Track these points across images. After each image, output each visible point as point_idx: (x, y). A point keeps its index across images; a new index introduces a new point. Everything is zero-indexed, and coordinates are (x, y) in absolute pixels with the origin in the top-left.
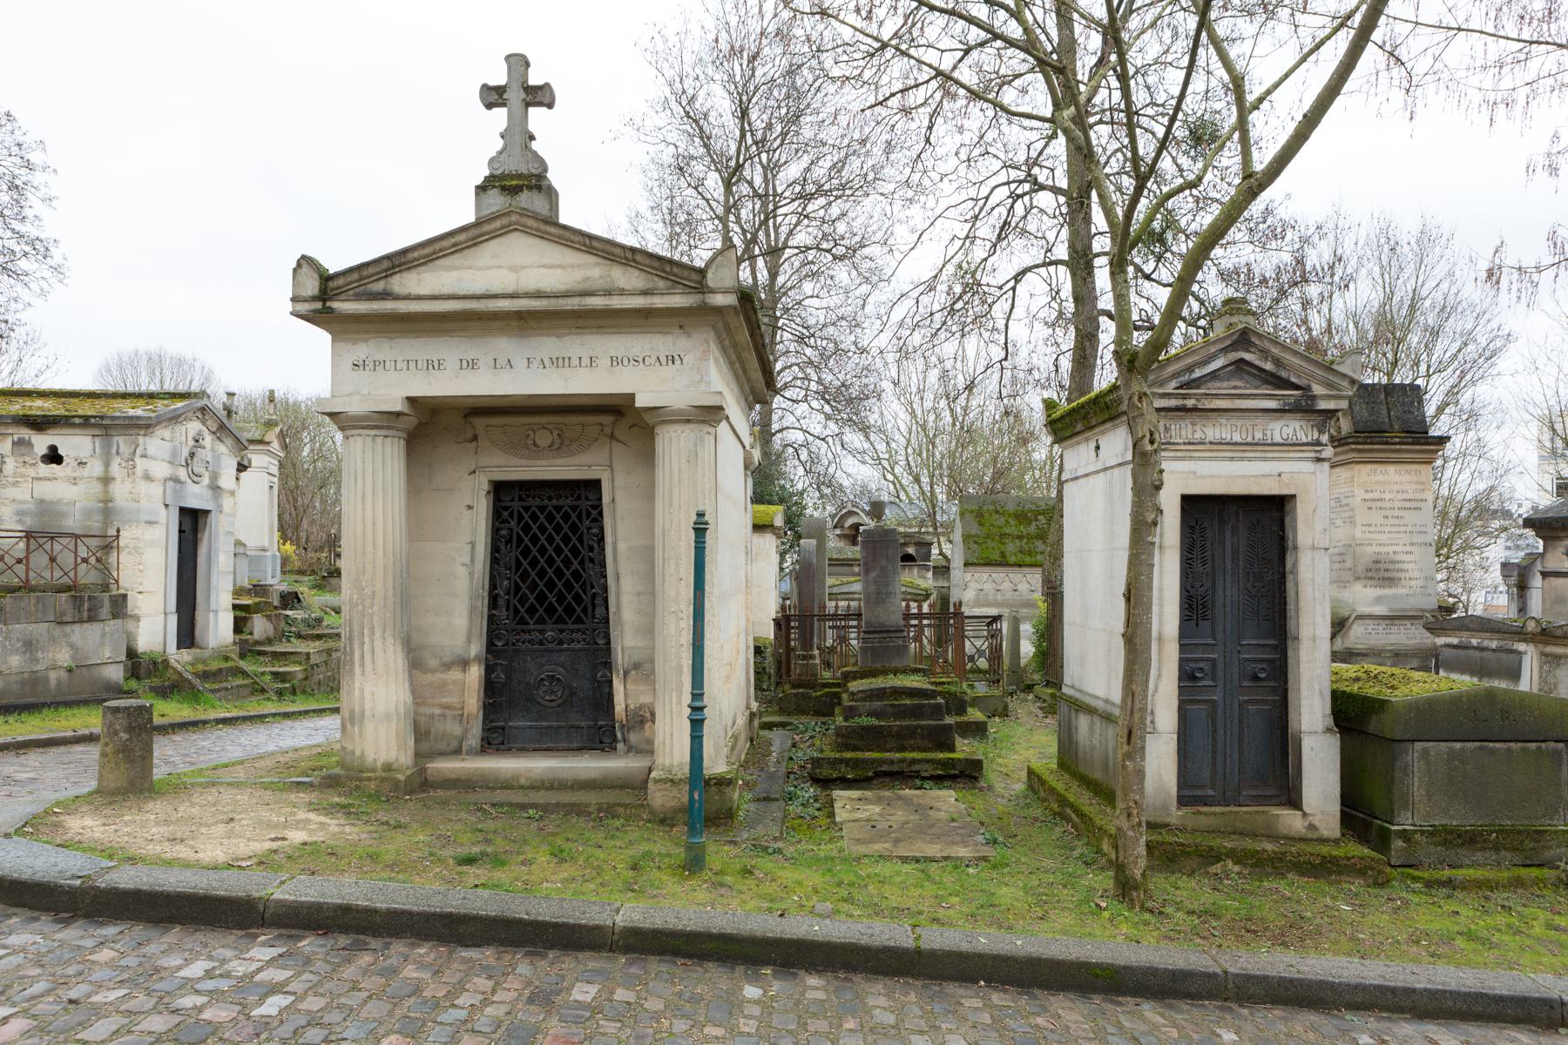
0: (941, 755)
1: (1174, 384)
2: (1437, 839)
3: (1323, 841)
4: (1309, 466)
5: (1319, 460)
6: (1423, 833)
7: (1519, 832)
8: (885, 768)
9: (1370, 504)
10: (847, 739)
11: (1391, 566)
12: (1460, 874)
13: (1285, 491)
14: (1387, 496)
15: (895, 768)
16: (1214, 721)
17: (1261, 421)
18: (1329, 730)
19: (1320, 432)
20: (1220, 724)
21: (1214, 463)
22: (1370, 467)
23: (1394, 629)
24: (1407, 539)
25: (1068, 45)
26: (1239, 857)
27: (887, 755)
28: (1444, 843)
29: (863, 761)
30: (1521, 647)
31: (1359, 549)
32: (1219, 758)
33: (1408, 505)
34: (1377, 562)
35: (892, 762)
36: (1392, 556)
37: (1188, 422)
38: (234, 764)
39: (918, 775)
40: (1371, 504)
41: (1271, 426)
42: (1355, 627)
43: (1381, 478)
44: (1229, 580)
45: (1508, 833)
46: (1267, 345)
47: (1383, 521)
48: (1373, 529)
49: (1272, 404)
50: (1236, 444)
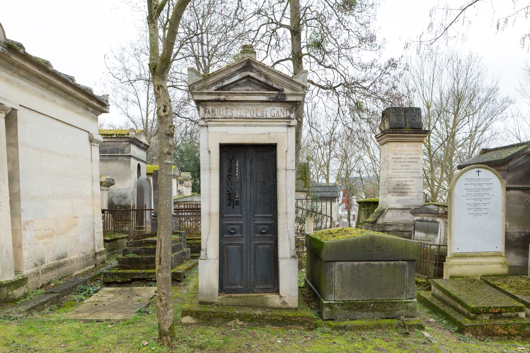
1: (214, 88)
4: (285, 129)
5: (289, 126)
6: (338, 304)
7: (384, 303)
8: (136, 277)
9: (395, 160)
10: (123, 264)
11: (404, 187)
12: (357, 322)
14: (403, 156)
15: (141, 277)
16: (242, 254)
17: (261, 107)
18: (293, 257)
19: (291, 112)
22: (395, 144)
23: (405, 214)
24: (411, 175)
26: (242, 317)
28: (348, 309)
29: (126, 274)
30: (438, 220)
31: (390, 179)
32: (244, 270)
33: (412, 160)
34: (398, 185)
35: (139, 274)
36: (404, 183)
37: (224, 107)
38: (457, 277)
39: (110, 275)
40: (396, 160)
41: (266, 109)
42: (388, 213)
43: (400, 148)
44: (249, 185)
45: (379, 303)
46: (260, 68)
47: (401, 167)
48: (396, 171)
49: (264, 98)
50: (248, 118)
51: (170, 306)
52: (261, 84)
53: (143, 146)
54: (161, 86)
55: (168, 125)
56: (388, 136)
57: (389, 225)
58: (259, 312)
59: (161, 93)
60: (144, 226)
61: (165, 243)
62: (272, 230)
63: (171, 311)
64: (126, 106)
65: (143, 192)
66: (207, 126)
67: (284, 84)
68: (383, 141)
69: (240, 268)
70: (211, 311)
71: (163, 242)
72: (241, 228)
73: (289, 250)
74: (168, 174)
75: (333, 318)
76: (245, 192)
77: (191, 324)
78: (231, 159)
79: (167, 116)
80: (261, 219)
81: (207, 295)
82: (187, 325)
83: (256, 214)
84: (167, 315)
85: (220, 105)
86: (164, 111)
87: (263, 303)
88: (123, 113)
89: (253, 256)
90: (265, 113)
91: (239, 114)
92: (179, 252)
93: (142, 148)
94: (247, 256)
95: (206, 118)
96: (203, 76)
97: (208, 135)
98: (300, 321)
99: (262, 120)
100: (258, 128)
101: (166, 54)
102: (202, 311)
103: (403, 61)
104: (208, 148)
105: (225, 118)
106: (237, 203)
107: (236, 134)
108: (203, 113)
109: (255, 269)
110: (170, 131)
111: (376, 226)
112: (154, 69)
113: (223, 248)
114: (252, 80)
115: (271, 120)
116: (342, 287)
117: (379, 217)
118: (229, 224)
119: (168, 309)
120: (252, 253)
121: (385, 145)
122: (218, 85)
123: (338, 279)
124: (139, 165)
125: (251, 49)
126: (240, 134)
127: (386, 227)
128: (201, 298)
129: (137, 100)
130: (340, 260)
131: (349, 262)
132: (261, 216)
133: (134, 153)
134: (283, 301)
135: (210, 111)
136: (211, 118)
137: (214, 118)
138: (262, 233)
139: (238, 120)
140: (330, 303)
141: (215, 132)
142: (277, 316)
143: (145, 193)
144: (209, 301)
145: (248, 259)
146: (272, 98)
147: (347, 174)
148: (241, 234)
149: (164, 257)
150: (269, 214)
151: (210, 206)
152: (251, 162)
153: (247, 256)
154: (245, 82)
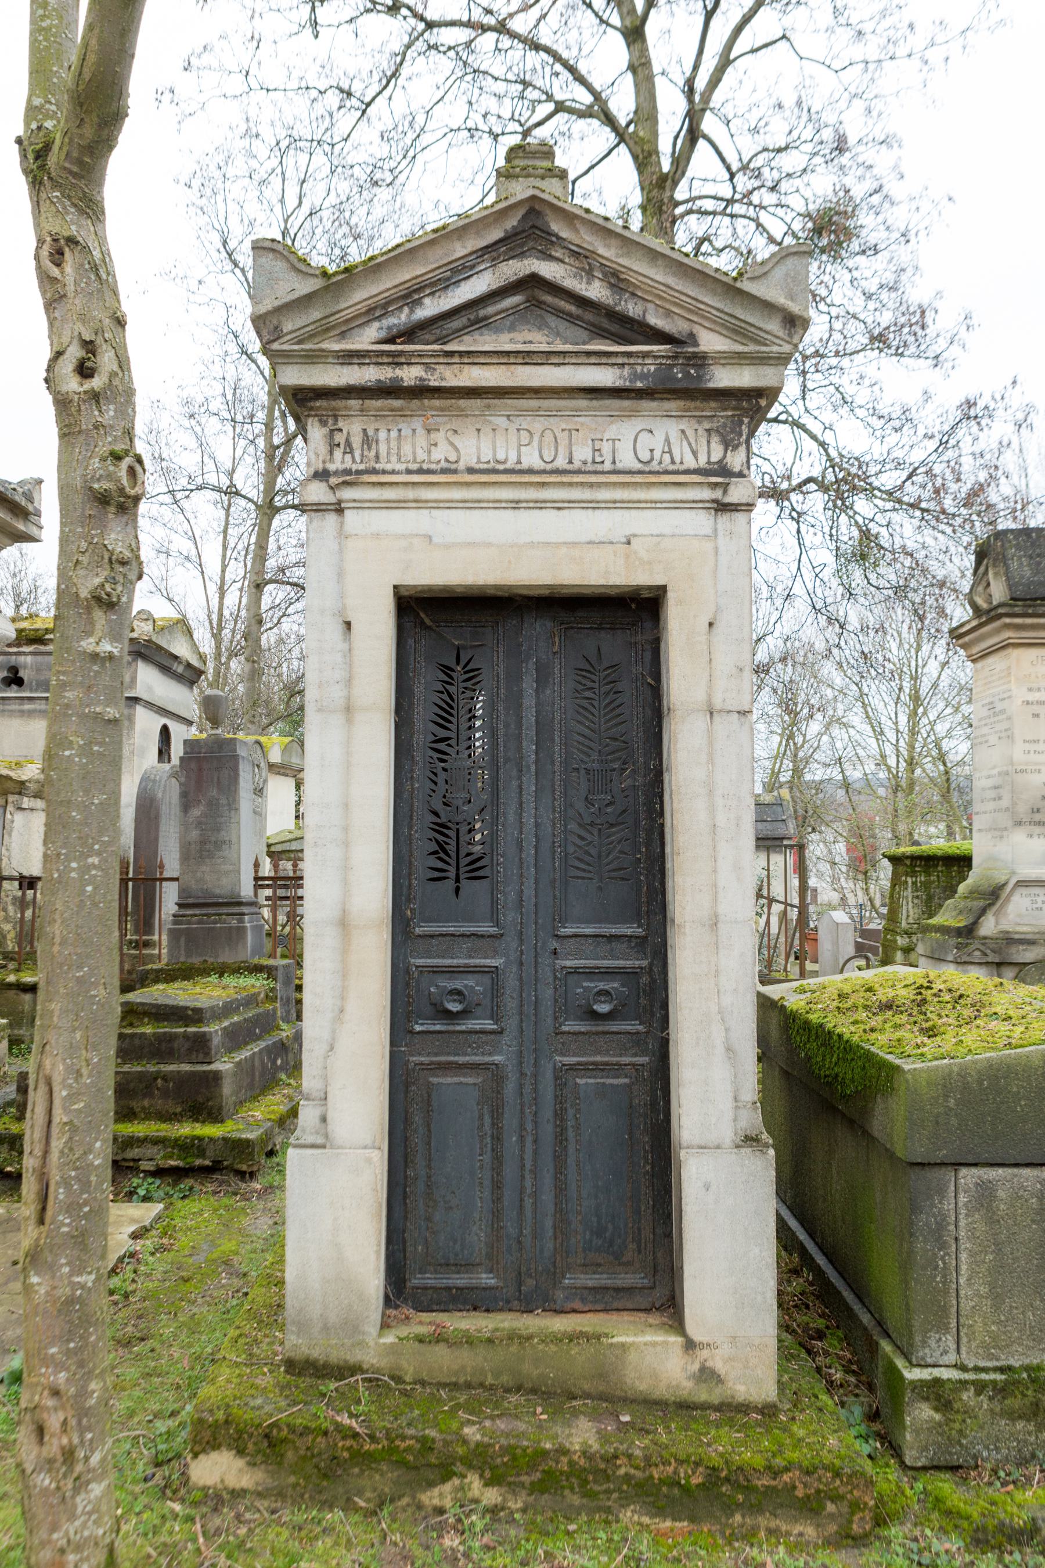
0: (186, 1130)
2: (1014, 1402)
3: (733, 1410)
4: (701, 521)
6: (980, 1387)
13: (642, 578)
16: (497, 1113)
18: (750, 1140)
20: (510, 1120)
21: (476, 516)
25: (647, 111)
26: (498, 1466)
27: (467, 1058)
31: (1020, 778)
32: (509, 1196)
37: (417, 423)
41: (614, 429)
42: (1016, 898)
44: (530, 786)
46: (588, 240)
50: (530, 471)
51: (95, 1459)
52: (589, 316)
53: (180, 669)
54: (72, 241)
55: (103, 449)
56: (1008, 626)
57: (1022, 942)
58: (582, 1435)
59: (70, 280)
60: (156, 937)
61: (71, 1098)
62: (643, 1001)
63: (97, 1489)
64: (163, 569)
65: (157, 817)
66: (339, 509)
67: (697, 312)
68: (984, 645)
69: (487, 1183)
70: (338, 1427)
71: (61, 1093)
72: (496, 990)
73: (729, 1104)
74: (97, 717)
75: (955, 1460)
76: (511, 817)
77: (237, 1494)
78: (452, 663)
79: (95, 396)
80: (587, 947)
81: (326, 1328)
82: (217, 1499)
83: (564, 921)
84: (72, 1517)
85: (401, 414)
86: (84, 371)
87: (602, 1376)
88: (154, 589)
89: (548, 1130)
90: (606, 448)
91: (487, 455)
92: (262, 1044)
93: (179, 678)
94: (522, 1127)
95: (336, 473)
96: (325, 274)
97: (341, 551)
98: (800, 1493)
99: (593, 479)
100: (578, 516)
101: (92, 58)
102: (292, 1429)
103: (1016, 399)
104: (342, 612)
105: (420, 471)
106: (476, 869)
107: (472, 544)
108: (323, 449)
109: (560, 1189)
110: (109, 477)
111: (976, 944)
112: (42, 154)
113: (407, 1085)
114: (549, 299)
115: (638, 479)
116: (997, 1298)
117: (983, 911)
118: (437, 971)
119: (80, 1484)
120: (548, 1113)
121: (990, 660)
122: (392, 321)
123: (972, 1254)
124: (165, 731)
125: (546, 164)
126: (489, 545)
127: (1013, 949)
128: (297, 1343)
129: (194, 552)
130: (986, 1156)
131: (1026, 1172)
132: (588, 931)
133: (150, 689)
134: (703, 1369)
135: (356, 441)
136: (358, 472)
137: (374, 471)
138: (595, 1016)
139: (484, 478)
140: (937, 1382)
141: (377, 536)
142: (681, 1462)
143: (163, 821)
144: (335, 1356)
145: (529, 1139)
146: (643, 377)
147: (797, 772)
148: (495, 1017)
149: (66, 1182)
150: (625, 921)
151: (345, 882)
152: (542, 680)
153: (522, 1127)
154: (514, 310)
